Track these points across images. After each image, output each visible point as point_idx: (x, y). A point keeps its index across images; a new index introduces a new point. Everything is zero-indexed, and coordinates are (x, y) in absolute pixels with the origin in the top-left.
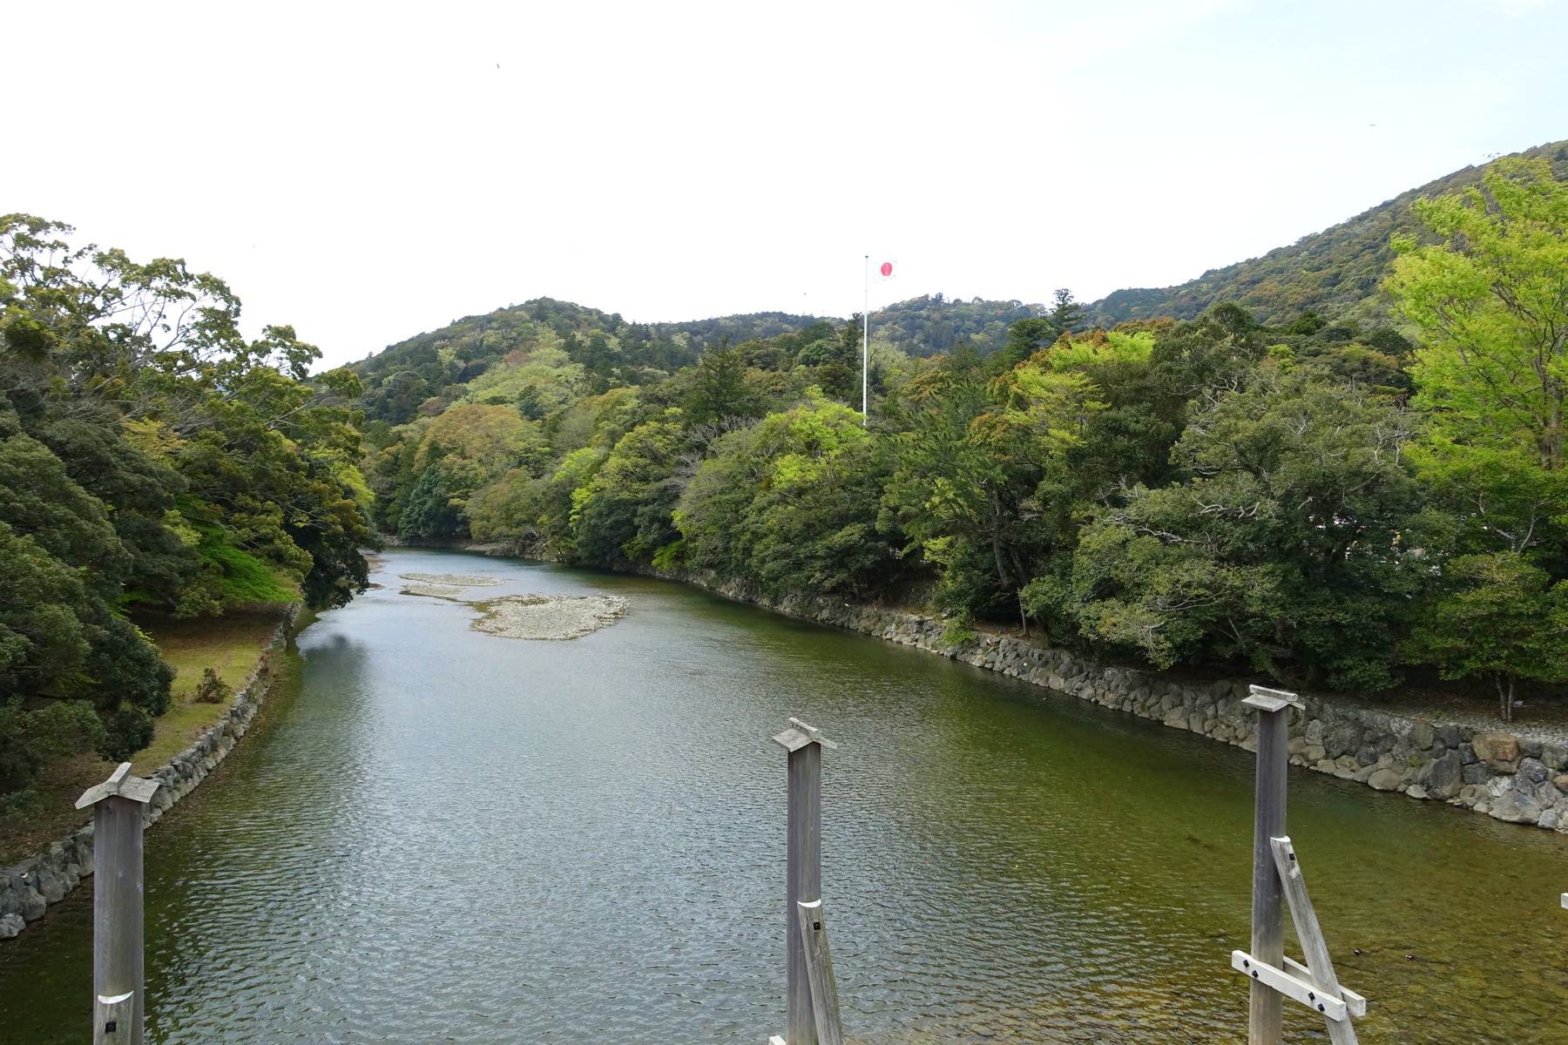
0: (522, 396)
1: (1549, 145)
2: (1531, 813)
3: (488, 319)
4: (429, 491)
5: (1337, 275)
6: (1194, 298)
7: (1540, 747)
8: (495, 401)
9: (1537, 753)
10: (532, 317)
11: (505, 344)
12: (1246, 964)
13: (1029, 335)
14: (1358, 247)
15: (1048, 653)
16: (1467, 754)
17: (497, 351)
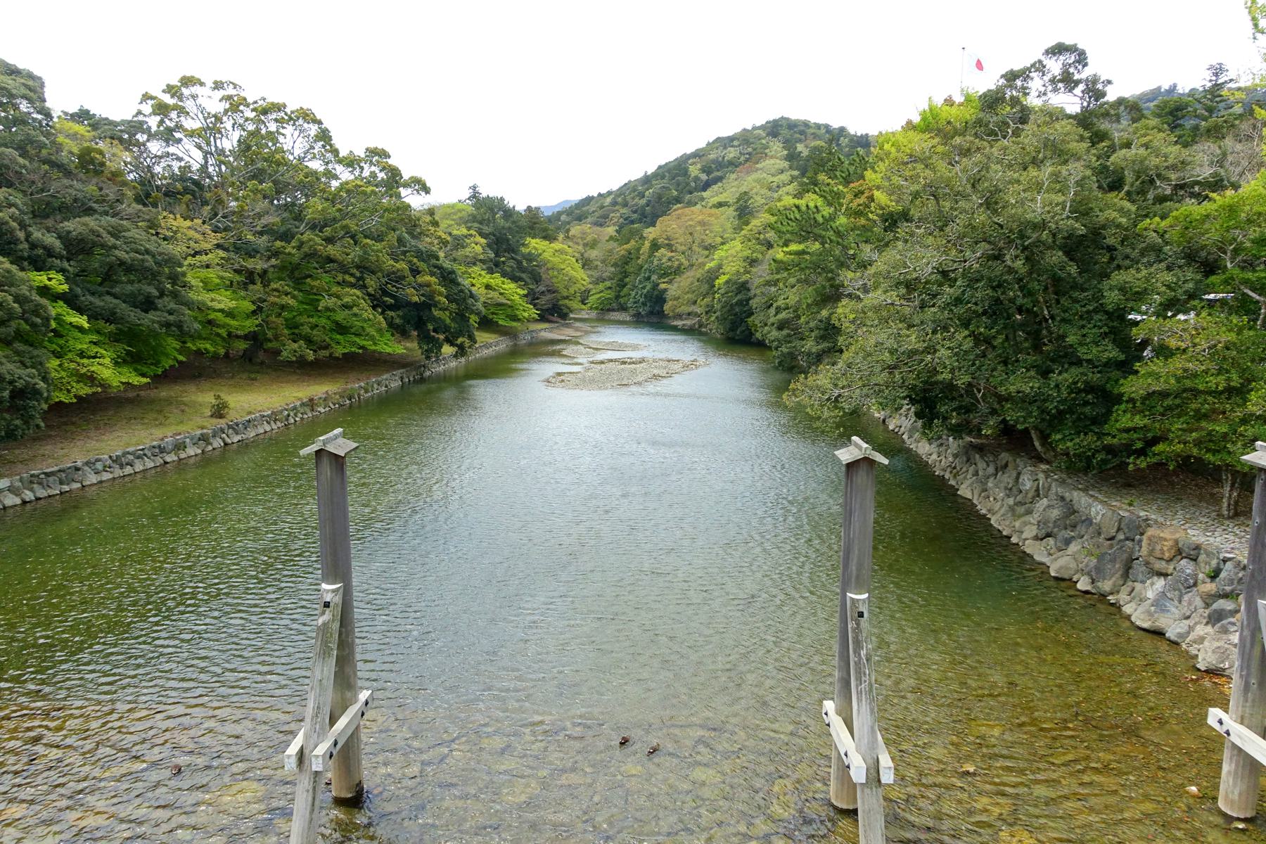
0: (738, 200)
2: (1163, 622)
3: (732, 139)
4: (649, 278)
7: (1198, 548)
8: (720, 205)
9: (1193, 553)
10: (768, 135)
11: (742, 159)
12: (1221, 722)
13: (1171, 113)
17: (733, 164)
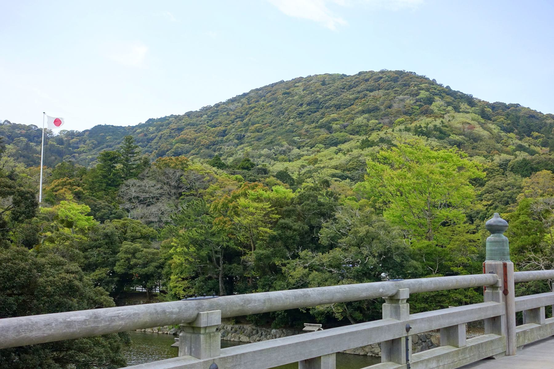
1: (316, 76)
5: (225, 131)
6: (146, 135)
13: (111, 160)
14: (234, 117)
15: (237, 326)
16: (429, 343)
